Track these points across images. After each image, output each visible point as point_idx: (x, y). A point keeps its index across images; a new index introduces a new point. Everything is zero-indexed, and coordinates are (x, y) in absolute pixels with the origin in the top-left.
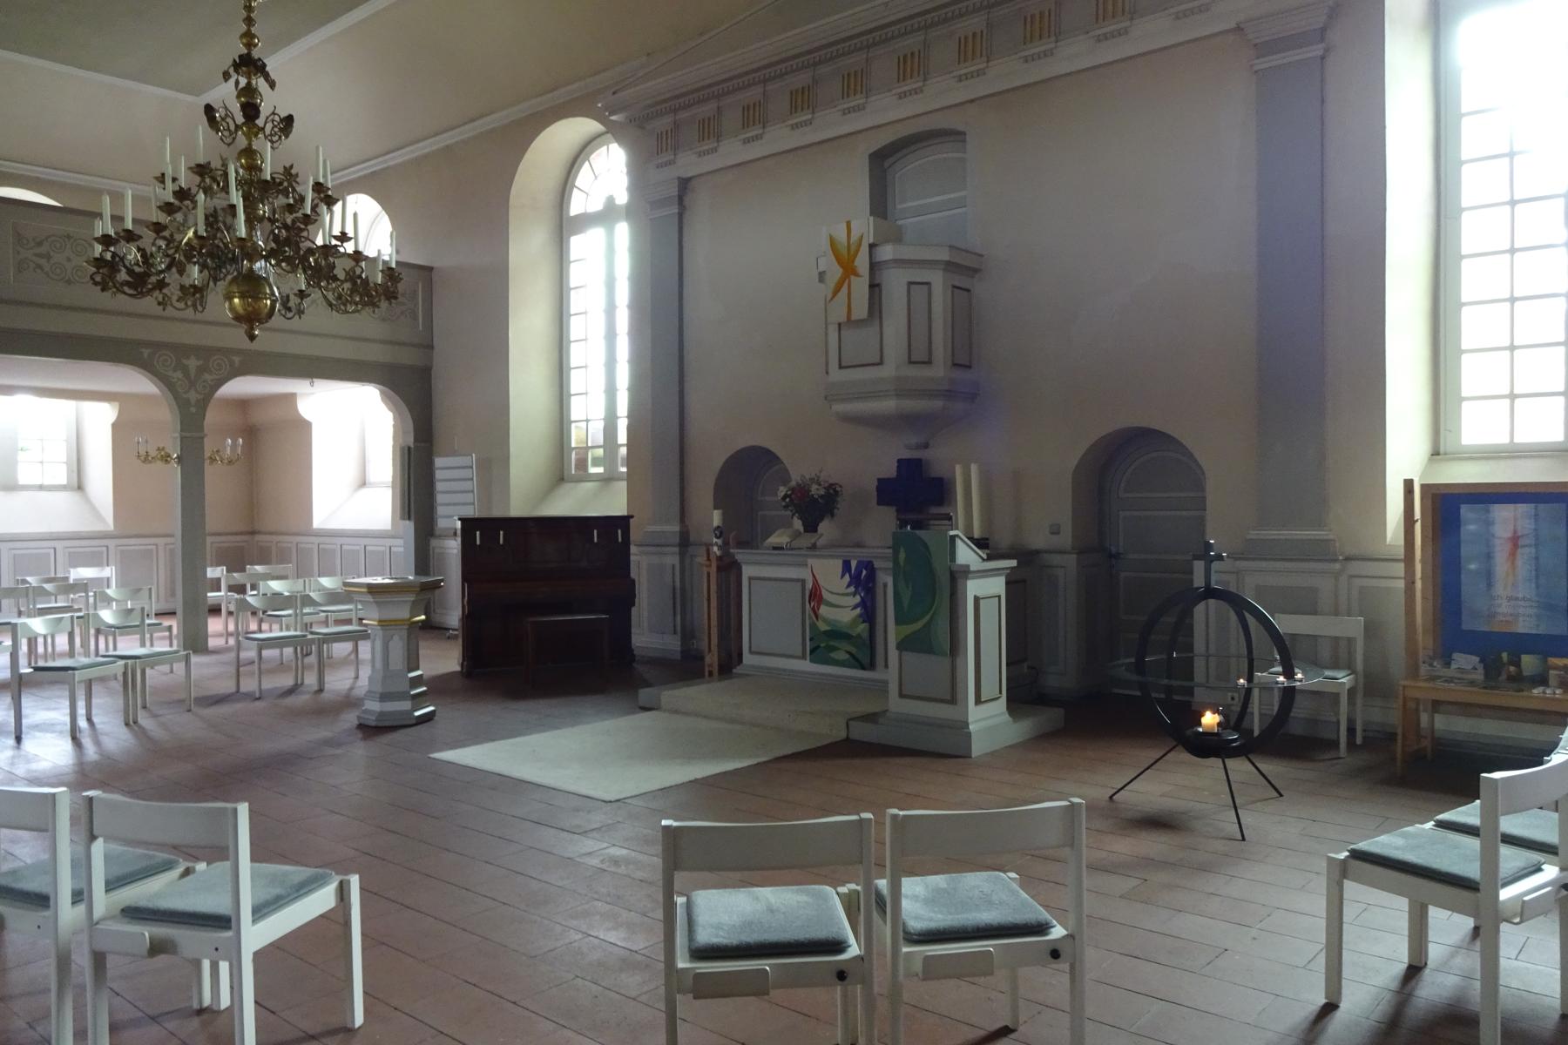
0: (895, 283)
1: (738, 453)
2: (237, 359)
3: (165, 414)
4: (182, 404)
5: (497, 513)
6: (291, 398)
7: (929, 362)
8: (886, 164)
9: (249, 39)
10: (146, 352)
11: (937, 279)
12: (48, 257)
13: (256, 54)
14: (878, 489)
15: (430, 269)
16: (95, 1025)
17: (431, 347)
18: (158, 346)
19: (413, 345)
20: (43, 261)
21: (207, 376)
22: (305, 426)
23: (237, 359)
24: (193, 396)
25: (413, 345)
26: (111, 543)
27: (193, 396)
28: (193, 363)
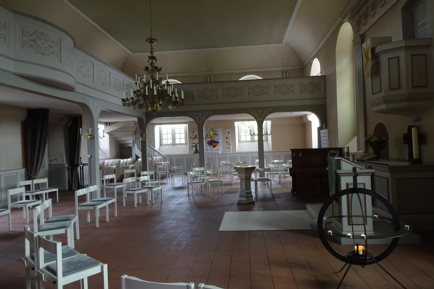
0: (384, 59)
1: (376, 126)
2: (270, 109)
3: (196, 126)
4: (198, 124)
5: (337, 147)
6: (306, 116)
7: (399, 88)
8: (413, 9)
9: (152, 52)
10: (190, 113)
11: (402, 54)
12: (203, 94)
13: (154, 55)
14: (404, 138)
15: (325, 76)
16: (37, 243)
17: (326, 98)
18: (252, 109)
19: (311, 99)
20: (228, 93)
21: (263, 114)
22: (310, 122)
23: (210, 112)
24: (200, 122)
25: (311, 99)
26: (271, 153)
27: (200, 122)
28: (200, 114)
